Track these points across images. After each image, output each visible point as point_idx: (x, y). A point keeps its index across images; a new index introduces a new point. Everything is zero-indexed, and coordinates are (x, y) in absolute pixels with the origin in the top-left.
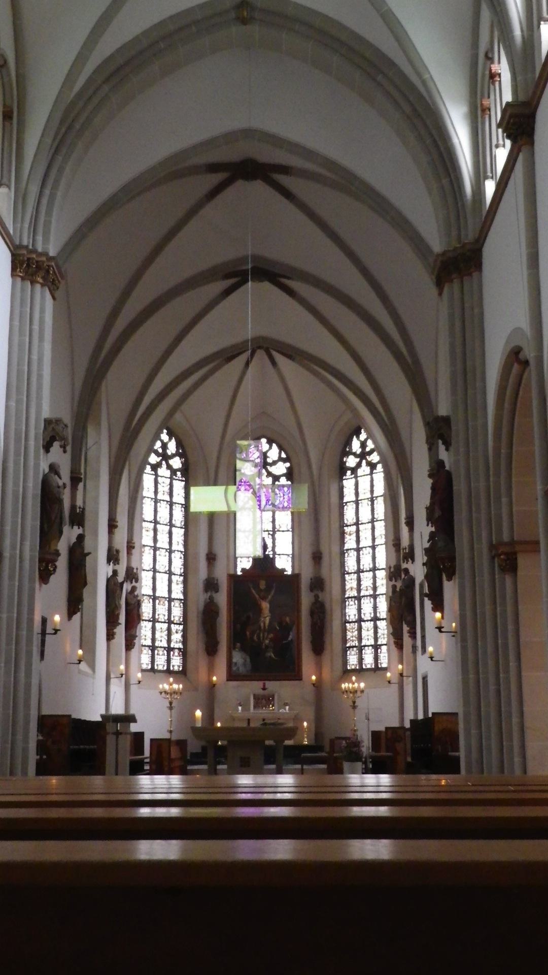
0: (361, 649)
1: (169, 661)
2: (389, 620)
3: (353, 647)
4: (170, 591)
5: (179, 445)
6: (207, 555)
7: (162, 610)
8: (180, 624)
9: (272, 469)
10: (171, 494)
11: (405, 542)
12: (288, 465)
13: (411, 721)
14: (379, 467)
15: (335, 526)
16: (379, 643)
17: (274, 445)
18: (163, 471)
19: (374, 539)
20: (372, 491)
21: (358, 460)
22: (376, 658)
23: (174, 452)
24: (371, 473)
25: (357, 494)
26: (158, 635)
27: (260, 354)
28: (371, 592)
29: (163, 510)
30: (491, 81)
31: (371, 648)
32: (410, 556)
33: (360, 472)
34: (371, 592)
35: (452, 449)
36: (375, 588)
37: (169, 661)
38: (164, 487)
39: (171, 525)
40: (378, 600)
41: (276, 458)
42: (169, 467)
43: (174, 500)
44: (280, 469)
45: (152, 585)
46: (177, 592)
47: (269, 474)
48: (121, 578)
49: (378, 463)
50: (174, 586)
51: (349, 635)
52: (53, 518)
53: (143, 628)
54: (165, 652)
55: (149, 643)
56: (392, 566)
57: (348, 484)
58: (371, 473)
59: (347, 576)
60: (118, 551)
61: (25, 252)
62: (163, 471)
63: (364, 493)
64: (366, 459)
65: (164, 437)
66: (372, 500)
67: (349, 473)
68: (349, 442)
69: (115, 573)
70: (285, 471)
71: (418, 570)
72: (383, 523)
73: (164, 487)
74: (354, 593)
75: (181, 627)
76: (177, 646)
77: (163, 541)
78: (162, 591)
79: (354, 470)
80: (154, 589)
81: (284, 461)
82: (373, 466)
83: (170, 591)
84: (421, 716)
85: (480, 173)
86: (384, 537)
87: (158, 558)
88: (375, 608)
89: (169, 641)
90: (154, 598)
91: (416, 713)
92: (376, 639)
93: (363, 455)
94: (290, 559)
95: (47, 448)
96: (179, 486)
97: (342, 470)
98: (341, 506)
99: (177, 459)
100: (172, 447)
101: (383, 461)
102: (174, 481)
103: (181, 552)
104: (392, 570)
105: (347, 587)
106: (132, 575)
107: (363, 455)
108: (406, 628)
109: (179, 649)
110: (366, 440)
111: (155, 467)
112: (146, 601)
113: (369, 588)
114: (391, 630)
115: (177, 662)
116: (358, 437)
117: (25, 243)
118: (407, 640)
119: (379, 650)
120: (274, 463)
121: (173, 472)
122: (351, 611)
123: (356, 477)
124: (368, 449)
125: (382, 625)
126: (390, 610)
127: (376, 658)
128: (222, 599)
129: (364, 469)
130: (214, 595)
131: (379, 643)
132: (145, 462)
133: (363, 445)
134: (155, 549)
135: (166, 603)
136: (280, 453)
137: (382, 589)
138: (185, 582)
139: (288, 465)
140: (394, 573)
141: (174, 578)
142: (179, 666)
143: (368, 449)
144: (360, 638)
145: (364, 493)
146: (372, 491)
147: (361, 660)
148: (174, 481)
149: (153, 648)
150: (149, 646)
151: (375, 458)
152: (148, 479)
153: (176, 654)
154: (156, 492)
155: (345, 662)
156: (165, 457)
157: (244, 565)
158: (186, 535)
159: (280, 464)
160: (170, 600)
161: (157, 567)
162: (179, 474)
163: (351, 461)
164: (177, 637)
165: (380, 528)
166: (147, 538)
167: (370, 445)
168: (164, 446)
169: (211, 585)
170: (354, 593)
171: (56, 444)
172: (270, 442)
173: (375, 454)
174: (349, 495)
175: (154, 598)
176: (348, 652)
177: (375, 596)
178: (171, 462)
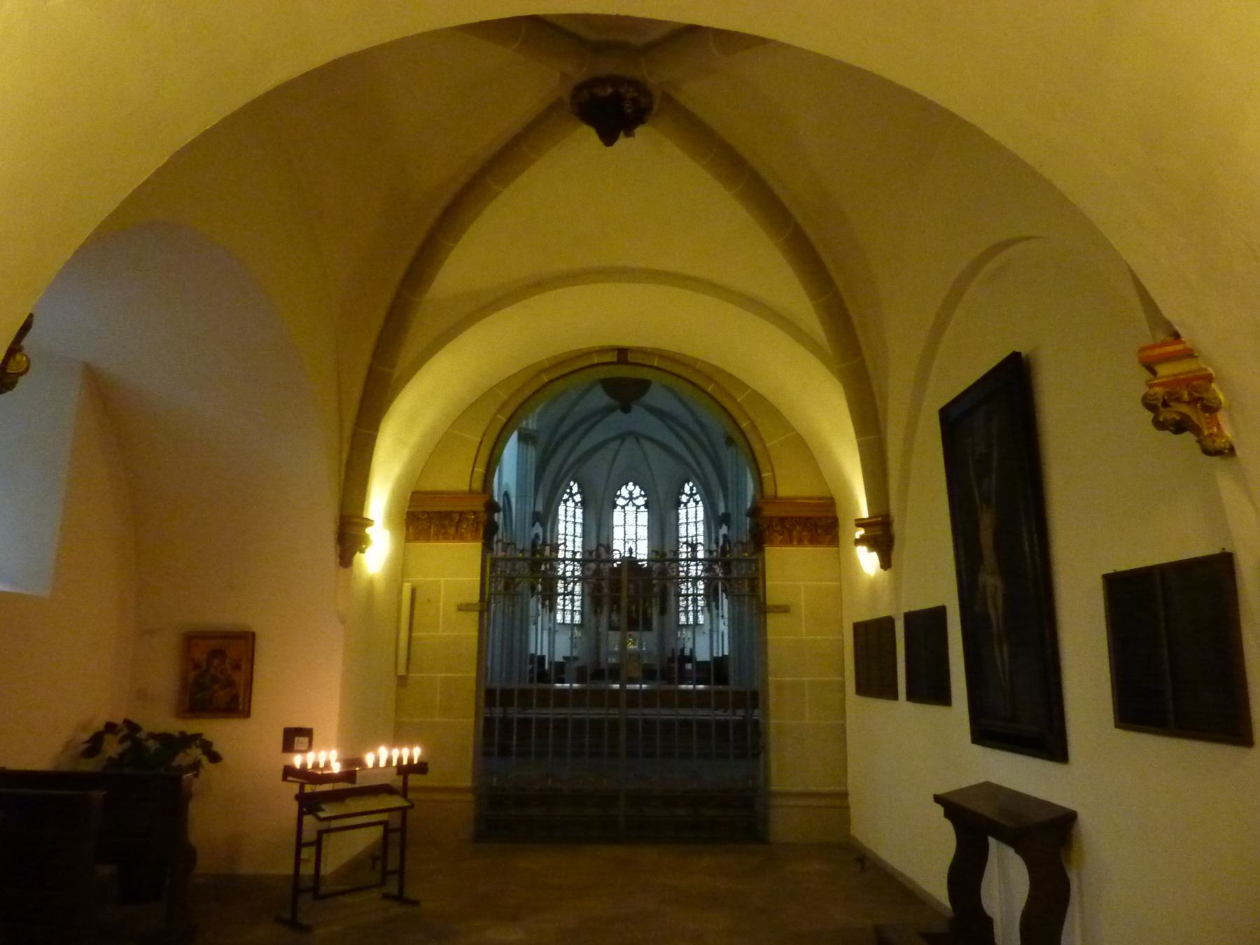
5: (579, 487)
9: (636, 502)
10: (574, 517)
12: (646, 499)
15: (673, 522)
17: (637, 487)
18: (570, 504)
20: (696, 518)
21: (688, 498)
24: (696, 507)
25: (687, 518)
27: (629, 442)
29: (570, 526)
33: (689, 505)
35: (681, 646)
38: (570, 513)
41: (638, 495)
42: (574, 501)
44: (641, 501)
57: (682, 512)
58: (696, 507)
62: (570, 504)
63: (692, 519)
66: (696, 523)
67: (682, 505)
70: (644, 503)
73: (570, 513)
75: (580, 598)
79: (686, 504)
81: (644, 496)
82: (697, 503)
84: (720, 655)
91: (723, 652)
93: (691, 495)
95: (533, 525)
97: (679, 503)
98: (677, 526)
99: (698, 495)
100: (575, 489)
101: (702, 500)
107: (691, 495)
108: (714, 604)
110: (693, 487)
111: (566, 501)
115: (577, 619)
118: (714, 611)
121: (576, 504)
123: (687, 508)
129: (692, 504)
132: (561, 499)
139: (646, 499)
145: (692, 519)
146: (696, 518)
151: (698, 497)
154: (566, 517)
155: (678, 619)
156: (571, 495)
159: (641, 498)
162: (579, 504)
171: (537, 524)
172: (635, 485)
174: (682, 519)
178: (575, 498)
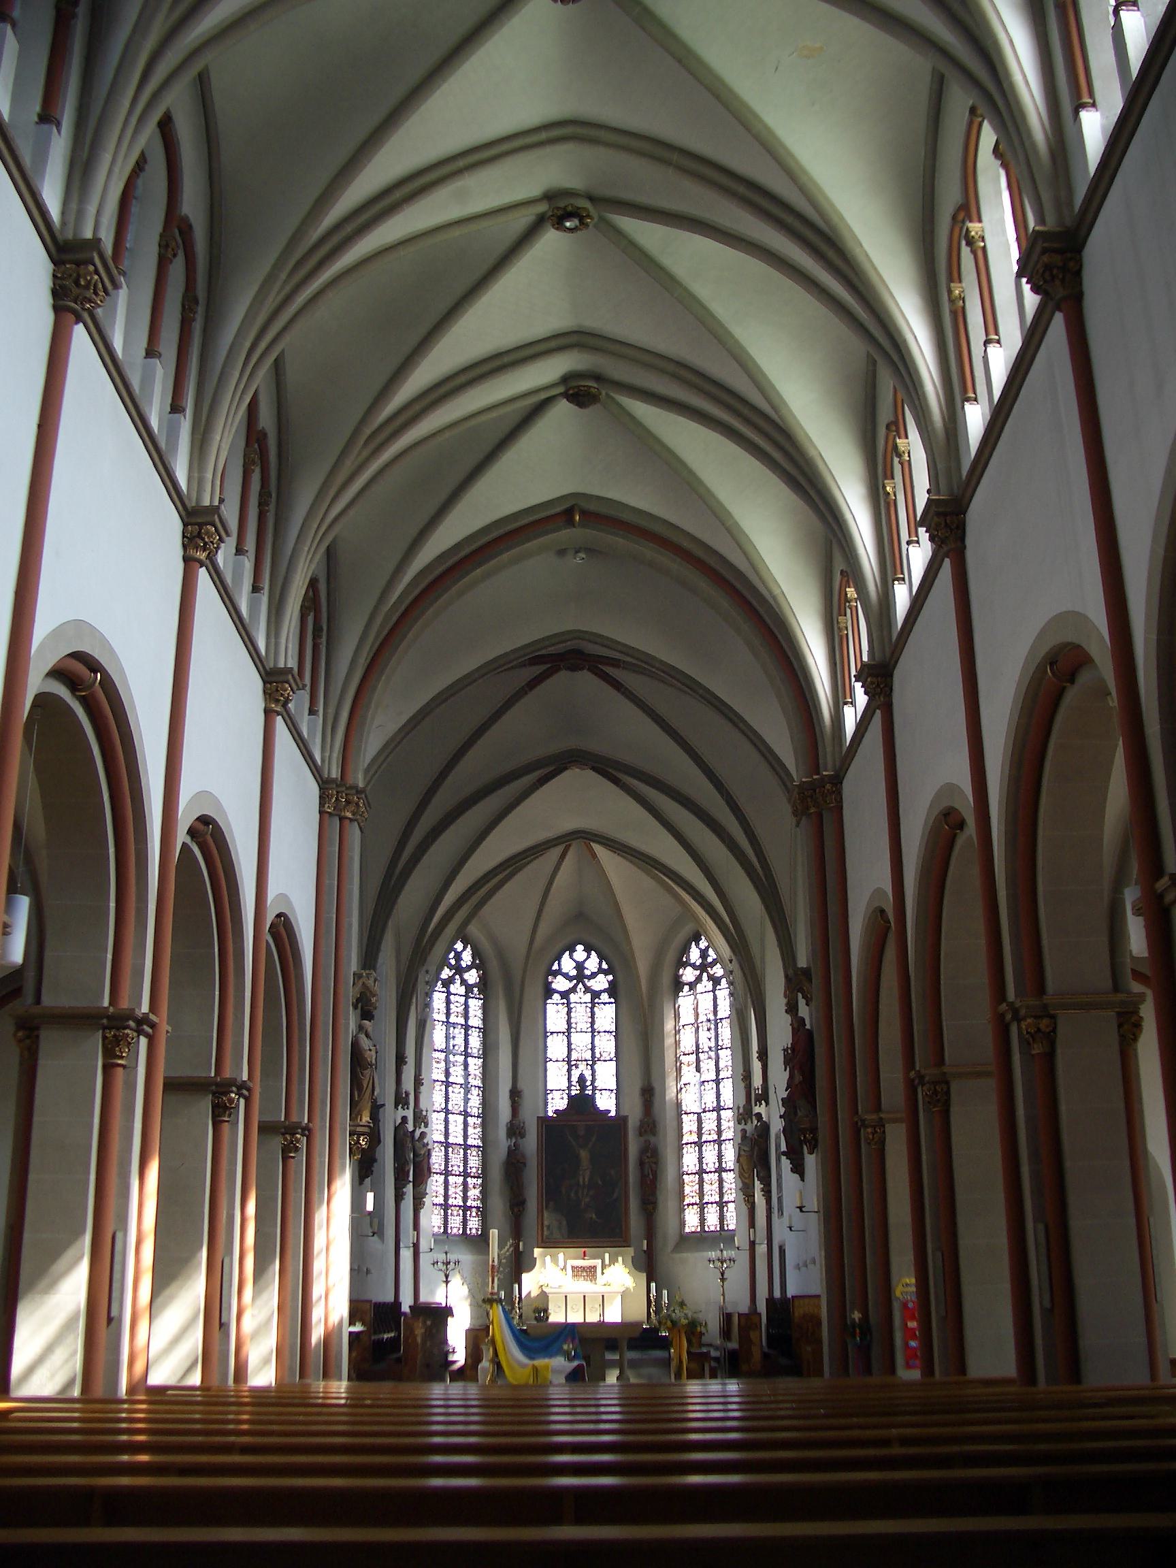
0: (702, 1206)
1: (465, 1222)
2: (737, 1170)
3: (693, 1204)
4: (466, 1136)
6: (511, 1091)
7: (456, 1160)
8: (478, 1177)
10: (466, 1016)
11: (757, 1081)
12: (610, 977)
13: (770, 1301)
14: (724, 981)
16: (725, 1199)
17: (593, 952)
19: (718, 1071)
20: (715, 1012)
21: (698, 972)
22: (722, 1218)
23: (469, 963)
26: (451, 1191)
28: (716, 1137)
30: (847, 604)
31: (715, 1205)
32: (764, 1097)
33: (700, 988)
34: (716, 1137)
36: (719, 1133)
37: (465, 1222)
38: (457, 1008)
39: (467, 1055)
40: (723, 1147)
42: (464, 982)
43: (470, 1023)
44: (601, 983)
45: (443, 1130)
46: (474, 1139)
47: (587, 989)
48: (410, 1127)
49: (722, 977)
50: (470, 1130)
51: (687, 1190)
52: (365, 1086)
53: (434, 1183)
54: (461, 1212)
55: (441, 1200)
56: (741, 1106)
57: (685, 1002)
59: (684, 1116)
60: (407, 1094)
61: (334, 786)
64: (708, 973)
65: (459, 946)
67: (686, 988)
68: (686, 950)
69: (404, 1119)
71: (773, 1114)
72: (729, 1052)
73: (457, 1008)
74: (694, 1138)
75: (480, 1181)
76: (474, 1204)
77: (457, 1075)
78: (456, 1137)
79: (692, 986)
80: (447, 1135)
81: (606, 972)
82: (716, 981)
83: (466, 1136)
85: (841, 697)
86: (730, 1068)
87: (451, 1095)
88: (720, 1156)
89: (465, 1198)
90: (447, 1145)
92: (721, 1195)
93: (703, 968)
94: (613, 1096)
96: (475, 1005)
97: (678, 985)
100: (467, 958)
102: (470, 1000)
103: (479, 1087)
104: (741, 1110)
105: (684, 1131)
106: (421, 1119)
108: (758, 1185)
109: (478, 1208)
110: (707, 948)
111: (447, 983)
112: (437, 1149)
113: (712, 1132)
114: (741, 1185)
115: (474, 1224)
116: (697, 945)
117: (334, 775)
119: (725, 1209)
120: (594, 975)
121: (469, 988)
122: (690, 1160)
124: (710, 960)
125: (729, 1177)
126: (738, 1160)
127: (722, 1218)
128: (531, 1143)
129: (706, 985)
130: (520, 1141)
131: (725, 1199)
133: (704, 954)
134: (448, 1084)
135: (462, 1151)
136: (600, 964)
137: (728, 1134)
138: (484, 1125)
139: (610, 977)
140: (744, 1115)
141: (471, 1120)
142: (477, 1229)
143: (710, 960)
144: (701, 1194)
146: (715, 1012)
147: (702, 1220)
148: (470, 1000)
149: (446, 1206)
150: (441, 1205)
151: (718, 971)
152: (438, 999)
153: (474, 1214)
154: (448, 1014)
155: (682, 1223)
156: (459, 970)
157: (557, 1103)
158: (485, 1066)
160: (466, 1147)
161: (450, 1107)
162: (476, 990)
163: (689, 975)
164: (474, 1193)
165: (726, 1057)
166: (438, 1074)
167: (712, 955)
168: (458, 956)
169: (515, 1130)
170: (694, 1138)
172: (588, 950)
173: (718, 965)
174: (686, 1016)
175: (447, 1145)
176: (687, 1211)
177: (719, 1142)
